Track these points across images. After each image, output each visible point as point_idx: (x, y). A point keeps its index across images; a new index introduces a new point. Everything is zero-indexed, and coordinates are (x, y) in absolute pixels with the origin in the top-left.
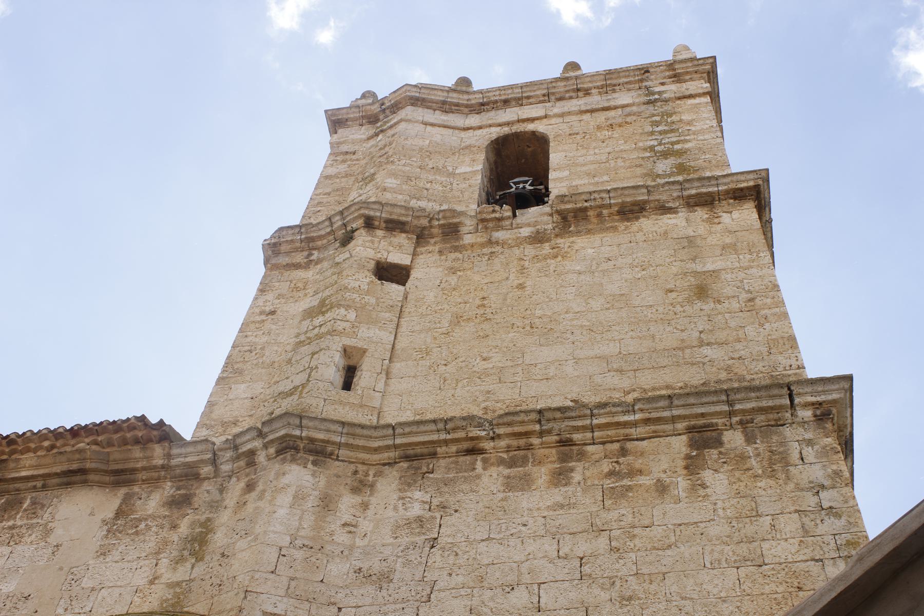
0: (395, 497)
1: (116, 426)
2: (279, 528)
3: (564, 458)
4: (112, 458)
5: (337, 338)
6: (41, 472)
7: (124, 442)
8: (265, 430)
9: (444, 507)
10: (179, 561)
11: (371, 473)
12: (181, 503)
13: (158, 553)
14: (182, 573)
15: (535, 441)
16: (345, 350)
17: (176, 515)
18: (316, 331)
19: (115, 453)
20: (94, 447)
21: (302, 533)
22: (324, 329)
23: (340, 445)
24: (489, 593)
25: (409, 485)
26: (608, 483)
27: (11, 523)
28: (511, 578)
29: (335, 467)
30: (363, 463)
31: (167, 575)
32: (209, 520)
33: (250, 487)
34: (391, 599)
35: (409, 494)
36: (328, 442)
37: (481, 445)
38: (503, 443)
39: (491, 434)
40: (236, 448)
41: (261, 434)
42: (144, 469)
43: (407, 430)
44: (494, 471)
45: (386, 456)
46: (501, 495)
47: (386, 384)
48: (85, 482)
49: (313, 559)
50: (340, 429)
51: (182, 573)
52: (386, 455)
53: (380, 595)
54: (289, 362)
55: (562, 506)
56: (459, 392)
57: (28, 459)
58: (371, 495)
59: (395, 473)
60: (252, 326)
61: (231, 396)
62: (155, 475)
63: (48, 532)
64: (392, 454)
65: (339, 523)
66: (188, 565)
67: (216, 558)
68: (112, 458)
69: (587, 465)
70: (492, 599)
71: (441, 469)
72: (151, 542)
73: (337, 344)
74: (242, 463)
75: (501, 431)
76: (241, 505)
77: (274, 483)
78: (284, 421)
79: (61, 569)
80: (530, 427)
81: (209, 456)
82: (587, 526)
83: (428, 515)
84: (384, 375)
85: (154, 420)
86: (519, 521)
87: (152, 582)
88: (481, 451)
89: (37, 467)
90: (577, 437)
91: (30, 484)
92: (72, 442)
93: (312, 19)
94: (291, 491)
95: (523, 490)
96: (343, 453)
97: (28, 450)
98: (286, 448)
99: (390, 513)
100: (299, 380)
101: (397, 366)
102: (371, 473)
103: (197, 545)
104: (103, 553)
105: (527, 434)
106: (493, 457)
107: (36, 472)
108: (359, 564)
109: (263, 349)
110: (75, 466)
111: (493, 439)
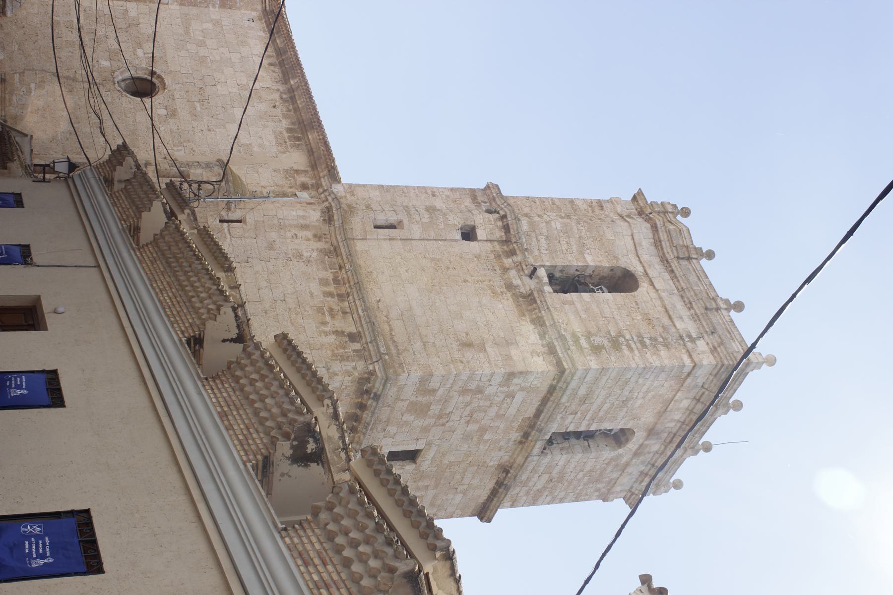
2: (286, 213)
15: (347, 285)
38: (345, 276)
90: (351, 297)
105: (349, 282)
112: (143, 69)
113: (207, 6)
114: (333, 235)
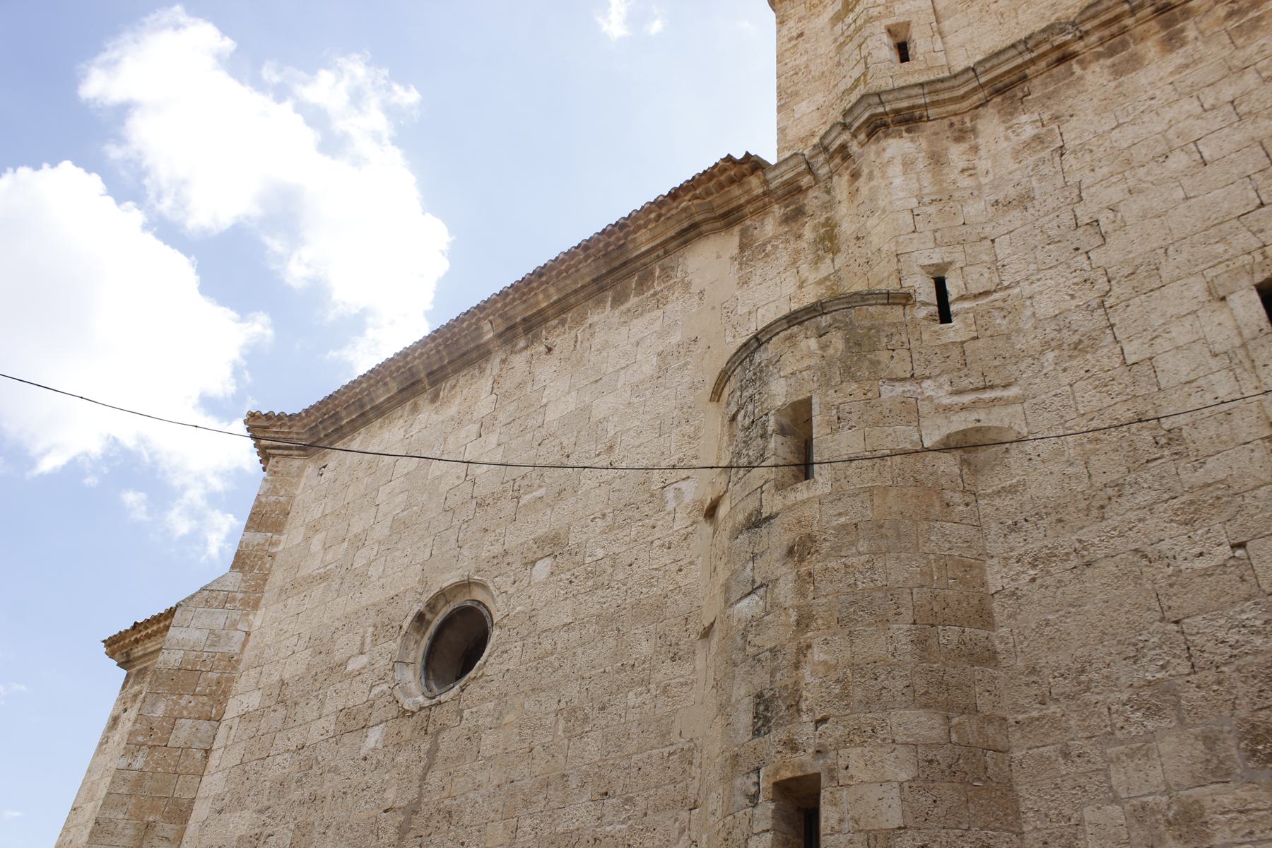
0: (1002, 128)
1: (708, 175)
2: (901, 195)
3: (1167, 25)
4: (715, 205)
5: (877, 23)
6: (658, 241)
7: (721, 186)
8: (848, 120)
9: (1057, 118)
10: (818, 260)
11: (967, 120)
12: (795, 216)
13: (794, 263)
14: (826, 268)
16: (889, 31)
17: (795, 228)
18: (853, 27)
19: (716, 199)
20: (696, 202)
21: (926, 191)
22: (859, 22)
23: (926, 106)
24: (1142, 171)
25: (1011, 114)
26: (1232, 24)
27: (652, 292)
28: (1160, 149)
29: (929, 127)
30: (956, 114)
31: (812, 276)
32: (828, 219)
33: (855, 176)
34: (1041, 213)
35: (1015, 121)
36: (913, 107)
37: (1071, 49)
38: (1094, 38)
39: (1078, 34)
40: (826, 149)
41: (845, 127)
42: (748, 202)
43: (988, 65)
44: (1095, 67)
45: (975, 99)
46: (1113, 84)
47: (944, 43)
48: (700, 235)
49: (947, 209)
50: (921, 91)
51: (826, 268)
52: (975, 98)
53: (1028, 214)
54: (839, 64)
55: (1187, 66)
56: (1022, 18)
57: (642, 235)
58: (976, 137)
59: (991, 110)
60: (788, 54)
61: (797, 116)
62: (760, 204)
63: (687, 286)
64: (981, 95)
65: (956, 172)
66: (828, 261)
67: (852, 244)
68: (715, 205)
69: (1197, 19)
70: (1148, 173)
71: (1037, 87)
72: (784, 257)
73: (879, 28)
74: (838, 160)
75: (1088, 26)
76: (853, 194)
77: (878, 161)
78: (864, 104)
79: (713, 308)
80: (1118, 10)
81: (804, 166)
82: (1225, 71)
83: (1044, 130)
84: (937, 36)
85: (739, 156)
86: (1145, 97)
87: (801, 287)
88: (1073, 55)
89: (654, 238)
91: (654, 255)
92: (675, 204)
93: (636, 19)
94: (898, 161)
95: (1134, 70)
96: (932, 112)
97: (639, 228)
98: (876, 127)
99: (1005, 144)
100: (856, 73)
101: (946, 25)
102: (967, 120)
103: (829, 240)
104: (744, 282)
105: (1117, 18)
106: (1088, 55)
107: (654, 244)
108: (993, 198)
109: (807, 67)
110: (686, 224)
111: (1081, 38)
112: (405, 647)
113: (272, 556)
114: (952, 108)
